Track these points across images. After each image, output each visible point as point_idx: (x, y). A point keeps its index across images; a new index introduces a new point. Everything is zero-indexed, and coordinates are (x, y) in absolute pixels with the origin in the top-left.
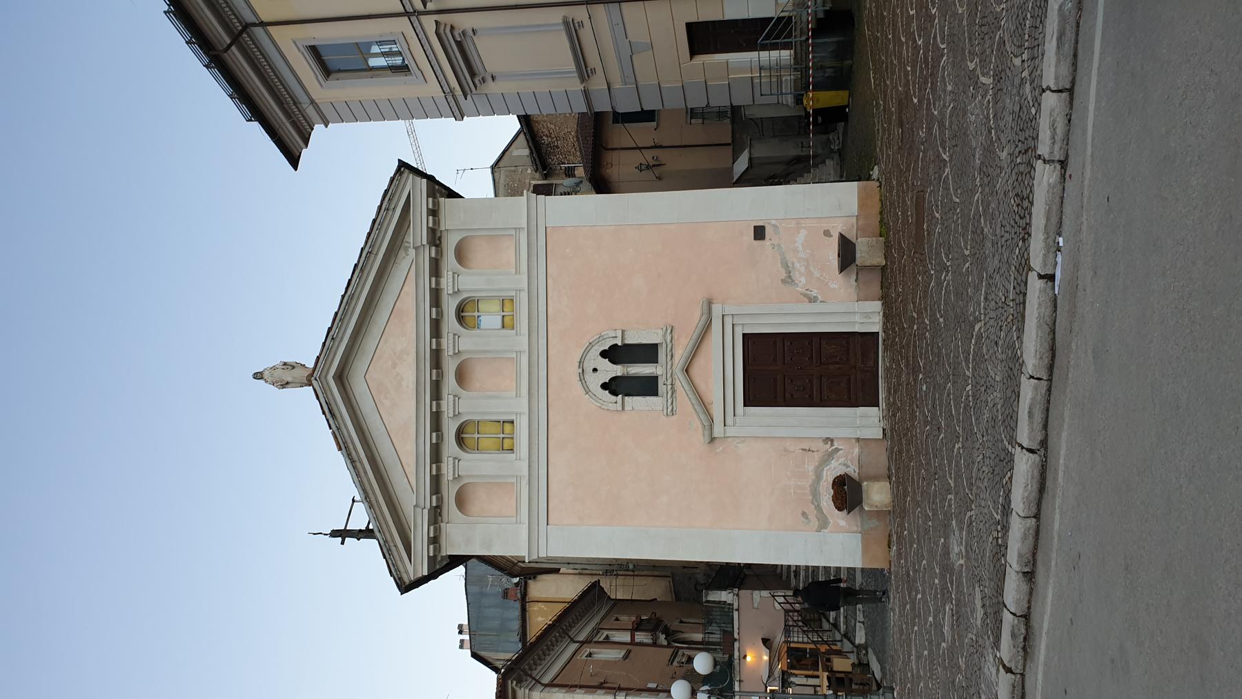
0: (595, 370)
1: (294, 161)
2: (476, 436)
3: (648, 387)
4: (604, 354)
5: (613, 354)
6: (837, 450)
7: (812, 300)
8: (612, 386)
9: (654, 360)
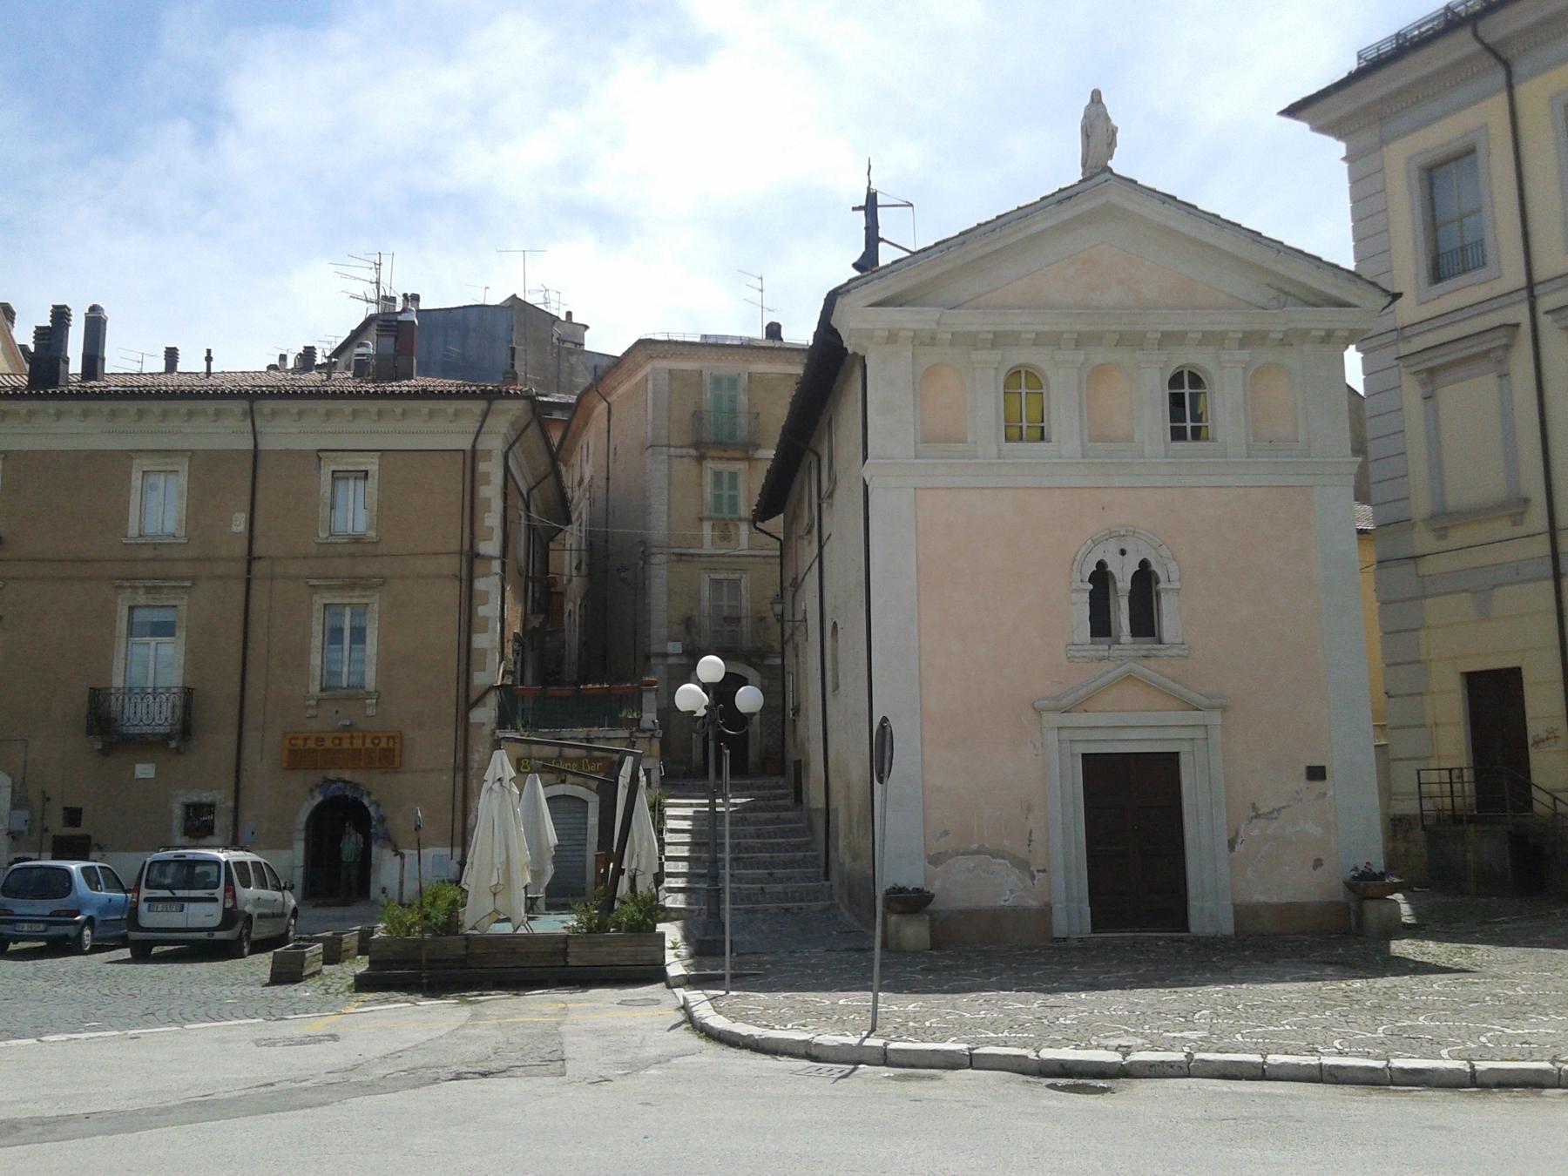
0: (1123, 552)
1: (1292, 111)
2: (1024, 391)
3: (1101, 625)
4: (1144, 564)
5: (1145, 578)
6: (1033, 877)
7: (1232, 845)
8: (1101, 578)
9: (1135, 632)
